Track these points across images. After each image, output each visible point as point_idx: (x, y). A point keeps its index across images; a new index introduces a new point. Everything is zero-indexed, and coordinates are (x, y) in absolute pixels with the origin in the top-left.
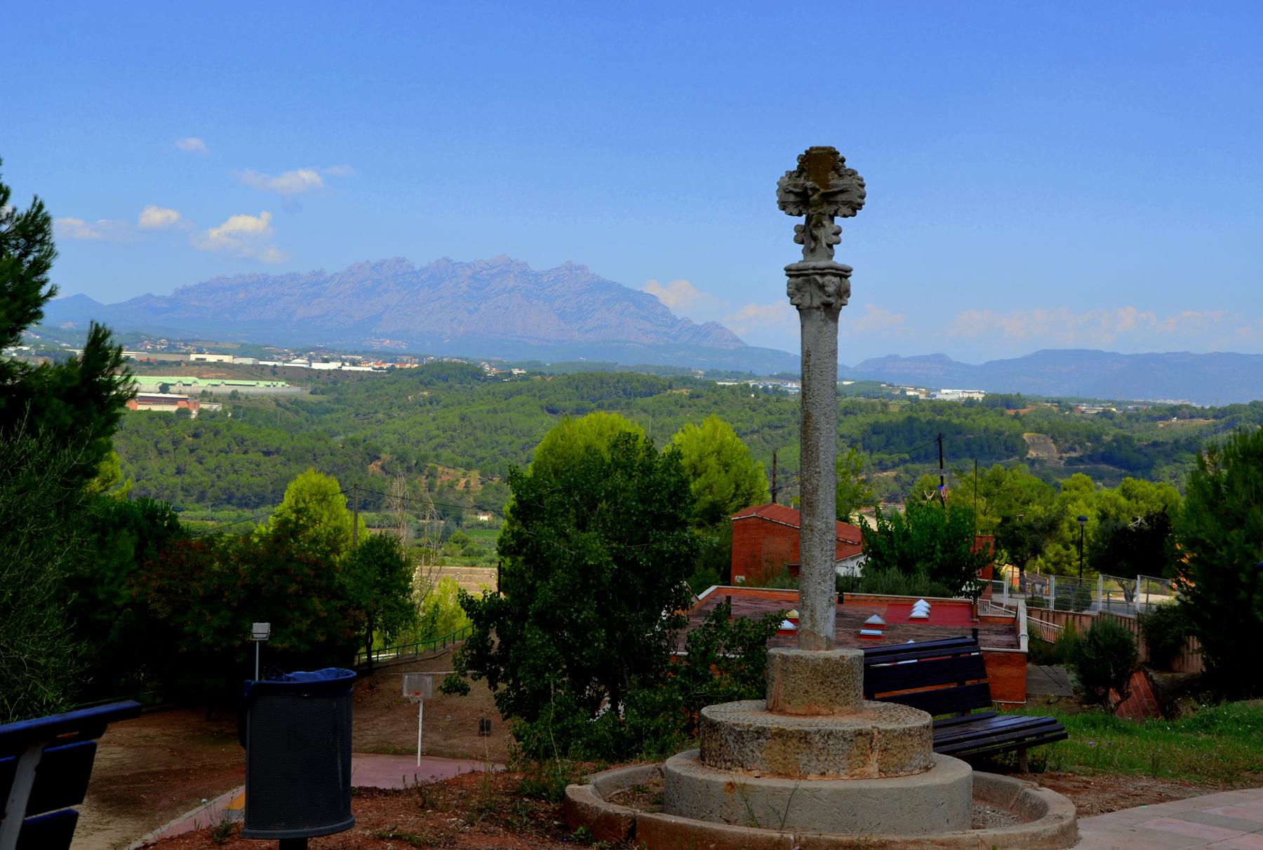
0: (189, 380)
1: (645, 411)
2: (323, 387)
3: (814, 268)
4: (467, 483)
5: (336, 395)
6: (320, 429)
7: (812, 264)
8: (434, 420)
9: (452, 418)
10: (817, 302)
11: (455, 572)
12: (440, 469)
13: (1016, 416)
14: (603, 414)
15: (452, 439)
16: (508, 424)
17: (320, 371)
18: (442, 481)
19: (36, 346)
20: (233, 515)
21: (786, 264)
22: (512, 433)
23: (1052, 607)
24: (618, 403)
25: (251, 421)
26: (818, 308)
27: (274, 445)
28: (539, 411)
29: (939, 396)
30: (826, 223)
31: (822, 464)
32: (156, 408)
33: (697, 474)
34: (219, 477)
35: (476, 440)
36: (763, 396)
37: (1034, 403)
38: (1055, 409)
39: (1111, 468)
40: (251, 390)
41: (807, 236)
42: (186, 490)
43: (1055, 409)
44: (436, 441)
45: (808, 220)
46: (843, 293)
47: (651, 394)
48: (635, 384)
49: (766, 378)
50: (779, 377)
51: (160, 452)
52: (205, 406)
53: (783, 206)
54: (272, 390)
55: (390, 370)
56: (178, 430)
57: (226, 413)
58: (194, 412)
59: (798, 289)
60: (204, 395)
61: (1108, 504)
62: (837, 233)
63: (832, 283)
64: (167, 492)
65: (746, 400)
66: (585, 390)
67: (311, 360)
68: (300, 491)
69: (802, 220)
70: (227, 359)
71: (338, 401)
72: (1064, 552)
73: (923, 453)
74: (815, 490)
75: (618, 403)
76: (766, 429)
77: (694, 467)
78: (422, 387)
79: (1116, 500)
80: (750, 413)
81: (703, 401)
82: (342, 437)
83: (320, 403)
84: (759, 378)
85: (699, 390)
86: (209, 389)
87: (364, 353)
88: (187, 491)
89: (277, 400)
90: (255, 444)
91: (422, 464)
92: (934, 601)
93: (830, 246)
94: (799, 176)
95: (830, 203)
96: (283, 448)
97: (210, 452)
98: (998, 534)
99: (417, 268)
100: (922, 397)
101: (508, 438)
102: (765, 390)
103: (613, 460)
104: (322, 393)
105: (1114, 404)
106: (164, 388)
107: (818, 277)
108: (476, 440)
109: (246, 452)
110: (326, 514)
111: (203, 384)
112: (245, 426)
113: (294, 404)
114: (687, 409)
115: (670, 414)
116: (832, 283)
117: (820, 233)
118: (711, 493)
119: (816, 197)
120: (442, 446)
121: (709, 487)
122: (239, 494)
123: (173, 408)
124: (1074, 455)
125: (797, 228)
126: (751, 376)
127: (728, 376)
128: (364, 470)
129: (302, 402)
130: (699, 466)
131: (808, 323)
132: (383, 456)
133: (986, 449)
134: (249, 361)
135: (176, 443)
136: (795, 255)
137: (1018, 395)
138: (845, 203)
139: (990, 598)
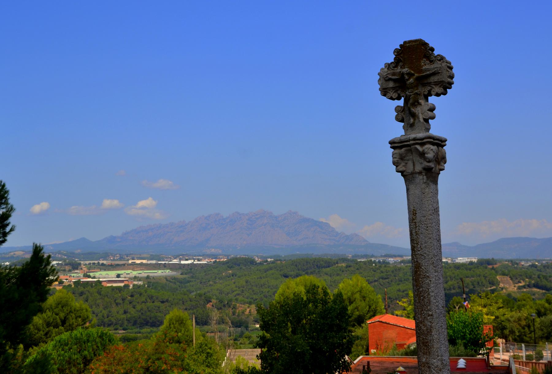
0: (129, 271)
1: (327, 274)
2: (186, 271)
3: (414, 139)
4: (250, 311)
5: (192, 275)
6: (185, 290)
7: (413, 136)
8: (234, 283)
9: (242, 282)
10: (418, 168)
11: (245, 352)
12: (238, 305)
13: (493, 268)
14: (307, 277)
15: (243, 291)
16: (267, 283)
17: (184, 265)
18: (239, 310)
19: (65, 261)
20: (149, 330)
21: (391, 138)
22: (269, 287)
23: (524, 360)
24: (314, 271)
25: (155, 288)
26: (420, 173)
27: (165, 298)
28: (280, 277)
29: (457, 261)
30: (422, 101)
31: (433, 307)
32: (115, 285)
33: (351, 303)
34: (142, 314)
35: (253, 291)
36: (378, 265)
37: (500, 261)
38: (510, 264)
39: (538, 290)
40: (155, 274)
41: (406, 115)
42: (128, 320)
43: (510, 264)
44: (236, 293)
45: (406, 102)
46: (441, 159)
47: (329, 267)
48: (322, 263)
49: (379, 257)
50: (385, 256)
51: (117, 304)
52: (135, 283)
53: (384, 92)
54: (164, 274)
55: (215, 262)
56: (125, 294)
57: (145, 285)
58: (131, 286)
59: (402, 158)
60: (135, 278)
61: (540, 307)
62: (432, 109)
63: (430, 151)
64: (120, 322)
65: (371, 267)
66: (300, 266)
67: (180, 260)
68: (171, 320)
69: (401, 103)
70: (144, 261)
71: (192, 277)
72: (522, 331)
73: (452, 287)
74: (429, 331)
75: (314, 271)
76: (381, 280)
77: (349, 299)
78: (229, 269)
79: (544, 305)
80: (373, 273)
81: (352, 268)
82: (195, 293)
83: (185, 278)
84: (376, 257)
85: (350, 264)
86: (137, 275)
87: (203, 256)
88: (129, 321)
89: (166, 278)
90: (157, 298)
91: (230, 303)
92: (468, 359)
93: (426, 121)
94: (396, 66)
95: (424, 85)
96: (169, 299)
97: (138, 303)
98: (494, 324)
99: (225, 217)
100: (449, 262)
101: (267, 290)
102: (379, 262)
103: (307, 298)
104: (186, 274)
105: (537, 261)
106: (118, 276)
107: (418, 147)
108: (253, 291)
109: (153, 302)
110: (183, 329)
111: (135, 273)
112: (153, 291)
113: (174, 280)
114: (345, 272)
115: (338, 275)
116: (430, 151)
117: (418, 110)
118: (358, 310)
119: (411, 80)
120: (238, 294)
121: (357, 308)
122: (151, 321)
123: (122, 285)
124: (520, 285)
125: (397, 109)
126: (373, 256)
127: (362, 257)
128: (205, 307)
129: (177, 278)
130: (351, 298)
131: (412, 187)
132: (213, 300)
133: (480, 284)
134: (154, 262)
135: (123, 300)
136: (398, 131)
137: (493, 259)
138: (437, 84)
139: (493, 356)
